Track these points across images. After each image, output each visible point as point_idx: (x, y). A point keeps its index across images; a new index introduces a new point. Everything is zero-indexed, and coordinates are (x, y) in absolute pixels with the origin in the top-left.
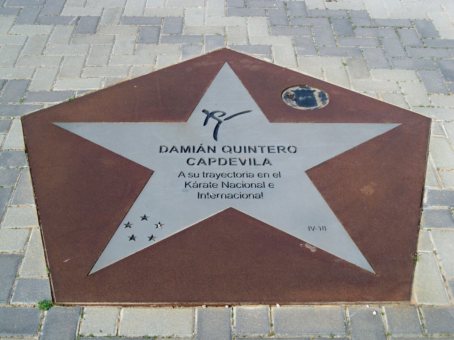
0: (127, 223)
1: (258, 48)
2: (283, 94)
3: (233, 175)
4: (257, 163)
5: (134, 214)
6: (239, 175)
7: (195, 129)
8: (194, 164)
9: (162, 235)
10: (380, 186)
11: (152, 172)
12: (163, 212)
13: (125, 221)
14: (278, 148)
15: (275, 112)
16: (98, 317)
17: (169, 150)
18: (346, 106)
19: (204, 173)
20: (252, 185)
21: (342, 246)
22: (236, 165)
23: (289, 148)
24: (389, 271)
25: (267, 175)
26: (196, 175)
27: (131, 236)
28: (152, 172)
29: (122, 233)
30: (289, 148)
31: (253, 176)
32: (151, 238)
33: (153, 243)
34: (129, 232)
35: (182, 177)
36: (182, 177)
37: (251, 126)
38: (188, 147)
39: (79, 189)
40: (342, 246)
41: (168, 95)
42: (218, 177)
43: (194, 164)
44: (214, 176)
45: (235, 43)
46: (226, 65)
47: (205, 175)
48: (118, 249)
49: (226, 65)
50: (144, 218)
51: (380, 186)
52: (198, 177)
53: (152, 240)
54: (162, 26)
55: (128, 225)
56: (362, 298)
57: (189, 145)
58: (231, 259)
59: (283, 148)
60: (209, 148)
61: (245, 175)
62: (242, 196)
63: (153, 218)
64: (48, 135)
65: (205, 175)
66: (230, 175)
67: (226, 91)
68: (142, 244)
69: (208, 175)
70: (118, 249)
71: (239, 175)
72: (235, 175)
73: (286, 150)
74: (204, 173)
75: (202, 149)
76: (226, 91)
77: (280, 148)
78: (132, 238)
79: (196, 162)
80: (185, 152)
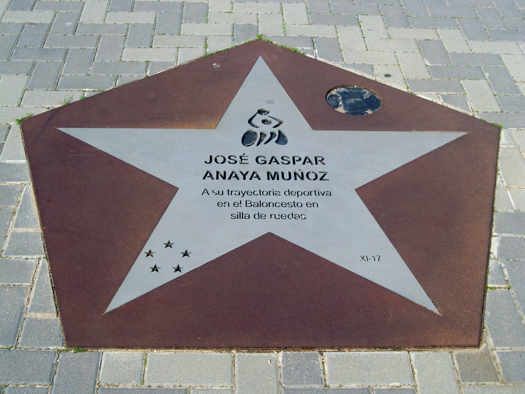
0: (148, 251)
1: (362, 66)
2: (349, 102)
5: (155, 241)
6: (265, 193)
7: (224, 136)
10: (435, 207)
11: (359, 191)
13: (146, 249)
15: (320, 118)
16: (117, 362)
17: (268, 162)
19: (228, 191)
20: (269, 203)
21: (387, 269)
24: (455, 319)
25: (315, 205)
26: (221, 193)
27: (176, 267)
28: (359, 191)
29: (142, 264)
31: (249, 218)
32: (178, 269)
33: (178, 274)
34: (151, 262)
35: (205, 194)
36: (205, 194)
38: (275, 173)
39: (88, 207)
40: (387, 269)
42: (244, 195)
44: (239, 194)
45: (271, 30)
48: (137, 283)
50: (168, 245)
51: (435, 207)
52: (223, 194)
55: (149, 254)
56: (505, 344)
57: (276, 171)
58: (272, 297)
59: (321, 159)
60: (218, 173)
61: (271, 193)
62: (260, 216)
64: (48, 143)
66: (255, 193)
67: (261, 90)
68: (167, 275)
70: (137, 283)
71: (265, 193)
72: (261, 193)
74: (228, 191)
75: (309, 160)
76: (261, 90)
77: (318, 159)
78: (155, 269)
80: (273, 179)
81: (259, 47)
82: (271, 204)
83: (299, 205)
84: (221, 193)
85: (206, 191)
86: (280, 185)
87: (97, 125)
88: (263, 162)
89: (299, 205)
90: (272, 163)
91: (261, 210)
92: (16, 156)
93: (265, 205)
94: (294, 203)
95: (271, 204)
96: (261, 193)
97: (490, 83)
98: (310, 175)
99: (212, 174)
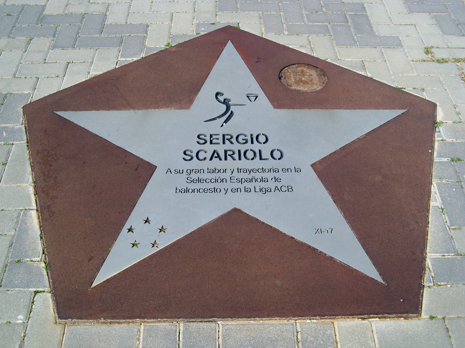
3: (262, 170)
4: (263, 158)
5: (135, 219)
6: (267, 171)
8: (205, 159)
9: (165, 242)
10: (381, 180)
11: (312, 166)
12: (159, 221)
13: (127, 226)
14: (224, 136)
15: (282, 97)
18: (342, 88)
19: (238, 169)
21: (347, 250)
22: (260, 151)
23: (237, 137)
24: (407, 303)
25: (224, 180)
26: (181, 172)
29: (124, 238)
30: (237, 137)
31: (250, 191)
33: (155, 250)
36: (169, 173)
37: (257, 114)
39: (82, 180)
40: (347, 250)
41: (170, 76)
43: (205, 159)
46: (230, 43)
47: (239, 171)
48: (121, 258)
49: (230, 43)
51: (381, 180)
53: (155, 247)
54: (281, 13)
57: (215, 149)
58: (231, 268)
63: (155, 224)
65: (239, 171)
67: (231, 73)
69: (242, 171)
70: (121, 258)
71: (267, 171)
73: (234, 140)
74: (238, 169)
76: (231, 73)
79: (209, 156)
81: (232, 34)
82: (196, 190)
83: (218, 190)
84: (181, 172)
85: (169, 170)
86: (230, 164)
87: (98, 270)
88: (244, 141)
89: (218, 190)
90: (214, 158)
91: (250, 185)
92: (18, 124)
93: (190, 191)
94: (214, 188)
95: (196, 190)
96: (263, 170)
97: (421, 297)
98: (252, 156)
99: (219, 153)
